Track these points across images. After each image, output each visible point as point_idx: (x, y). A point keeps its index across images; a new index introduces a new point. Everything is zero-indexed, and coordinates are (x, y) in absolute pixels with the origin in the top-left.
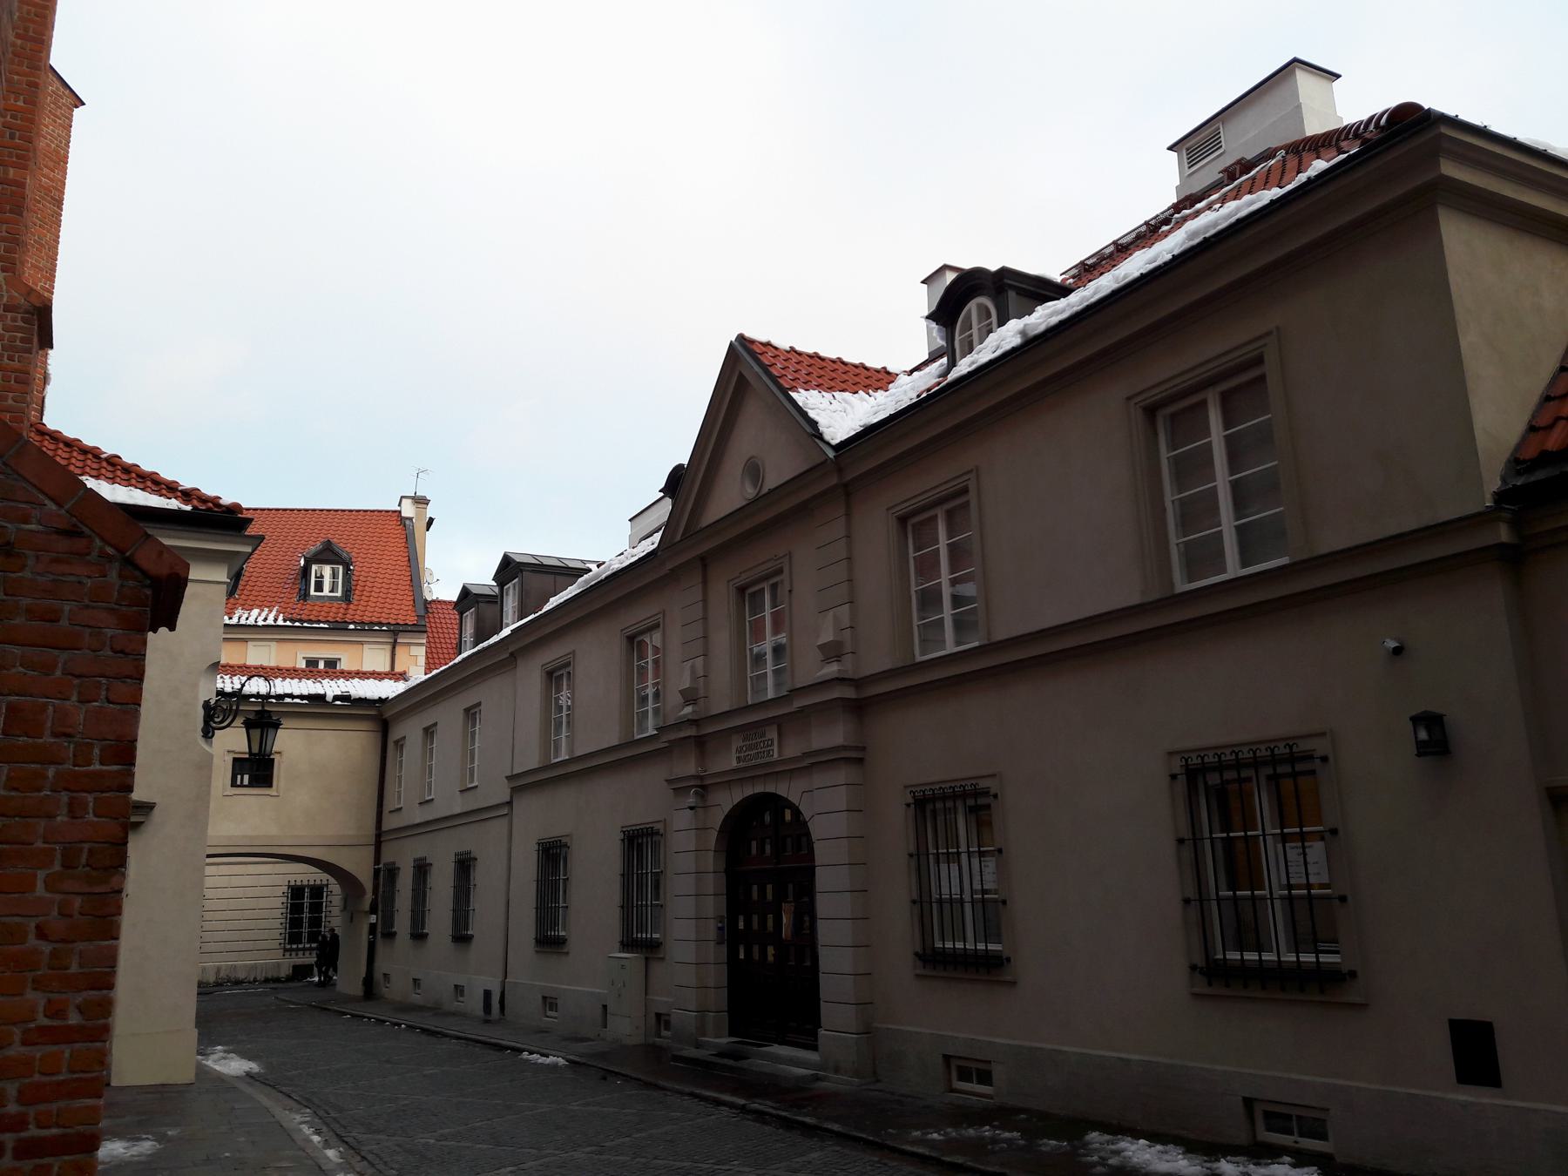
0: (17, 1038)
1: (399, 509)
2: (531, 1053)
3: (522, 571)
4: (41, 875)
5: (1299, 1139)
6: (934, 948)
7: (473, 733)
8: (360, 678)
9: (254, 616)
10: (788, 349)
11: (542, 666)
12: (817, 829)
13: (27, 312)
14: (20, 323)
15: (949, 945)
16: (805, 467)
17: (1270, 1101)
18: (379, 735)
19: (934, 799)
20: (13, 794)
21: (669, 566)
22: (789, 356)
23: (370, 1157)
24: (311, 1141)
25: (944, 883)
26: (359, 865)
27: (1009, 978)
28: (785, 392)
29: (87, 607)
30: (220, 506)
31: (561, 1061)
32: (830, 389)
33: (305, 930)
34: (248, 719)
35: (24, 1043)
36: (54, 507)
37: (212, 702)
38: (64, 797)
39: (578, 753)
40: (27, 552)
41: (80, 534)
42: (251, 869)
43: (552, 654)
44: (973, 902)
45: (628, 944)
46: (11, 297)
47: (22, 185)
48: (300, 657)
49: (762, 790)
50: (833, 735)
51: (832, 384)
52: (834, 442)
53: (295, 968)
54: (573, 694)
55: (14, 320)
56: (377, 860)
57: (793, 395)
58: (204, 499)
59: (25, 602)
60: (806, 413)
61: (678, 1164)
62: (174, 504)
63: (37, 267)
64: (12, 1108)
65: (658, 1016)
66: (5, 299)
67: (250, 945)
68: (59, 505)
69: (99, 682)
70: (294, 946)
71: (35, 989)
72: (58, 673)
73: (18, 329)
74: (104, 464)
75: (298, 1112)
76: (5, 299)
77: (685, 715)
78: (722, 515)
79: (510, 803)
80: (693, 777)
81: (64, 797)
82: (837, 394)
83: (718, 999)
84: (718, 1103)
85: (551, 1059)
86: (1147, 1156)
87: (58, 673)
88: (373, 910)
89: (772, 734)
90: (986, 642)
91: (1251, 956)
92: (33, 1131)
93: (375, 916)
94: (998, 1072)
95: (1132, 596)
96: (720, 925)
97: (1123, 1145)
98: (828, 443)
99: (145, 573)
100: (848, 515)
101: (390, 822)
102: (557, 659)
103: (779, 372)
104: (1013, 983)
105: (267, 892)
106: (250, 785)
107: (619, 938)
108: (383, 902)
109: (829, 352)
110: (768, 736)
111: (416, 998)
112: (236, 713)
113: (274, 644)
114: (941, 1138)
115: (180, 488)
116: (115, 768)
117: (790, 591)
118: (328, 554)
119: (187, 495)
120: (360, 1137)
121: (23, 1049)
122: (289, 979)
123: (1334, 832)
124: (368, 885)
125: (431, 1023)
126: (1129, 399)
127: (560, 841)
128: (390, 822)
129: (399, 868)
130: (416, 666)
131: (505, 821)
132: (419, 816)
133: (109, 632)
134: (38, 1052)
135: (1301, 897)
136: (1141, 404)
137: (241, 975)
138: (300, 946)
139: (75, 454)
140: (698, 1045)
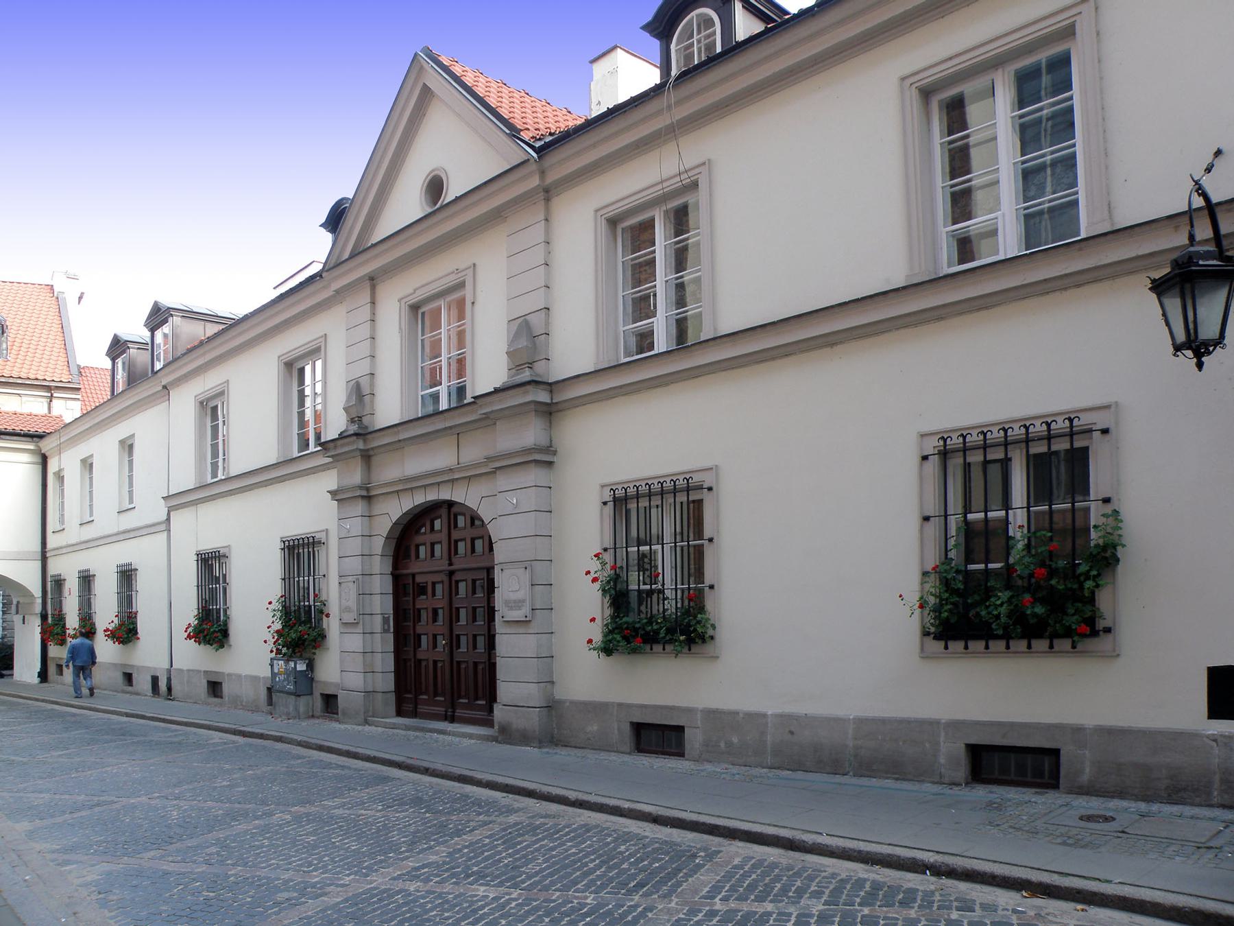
18: (39, 468)
19: (626, 499)
39: (170, 494)
101: (52, 541)
117: (473, 303)
126: (903, 79)
127: (219, 552)
129: (65, 580)
131: (166, 533)
136: (916, 85)
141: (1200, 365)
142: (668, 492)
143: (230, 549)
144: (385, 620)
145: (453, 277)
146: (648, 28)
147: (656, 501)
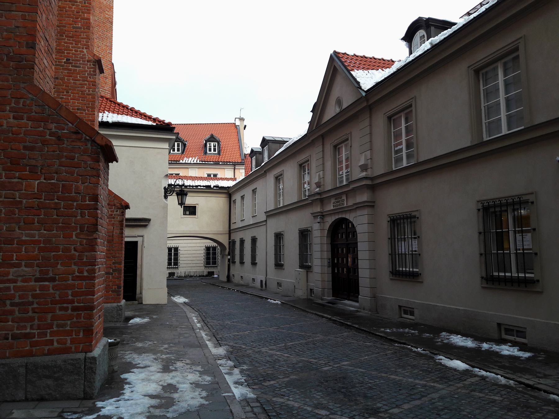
0: (70, 279)
1: (235, 122)
2: (271, 299)
3: (269, 143)
4: (74, 233)
5: (516, 338)
6: (396, 270)
7: (255, 198)
8: (222, 180)
9: (190, 160)
10: (353, 55)
12: (359, 229)
13: (94, 62)
14: (92, 66)
15: (401, 269)
16: (356, 99)
17: (507, 325)
18: (228, 199)
19: (397, 219)
20: (65, 210)
21: (311, 139)
22: (353, 57)
23: (209, 326)
24: (194, 321)
25: (400, 248)
26: (224, 240)
27: (421, 280)
28: (349, 71)
29: (82, 155)
30: (164, 123)
31: (279, 302)
32: (368, 69)
33: (211, 261)
34: (177, 192)
35: (72, 280)
36: (71, 125)
37: (167, 187)
38: (79, 211)
39: (285, 205)
40: (65, 139)
41: (79, 133)
42: (194, 241)
43: (276, 171)
44: (516, 254)
45: (302, 266)
46: (89, 58)
47: (89, 19)
48: (205, 173)
49: (345, 217)
50: (363, 197)
51: (369, 67)
52: (366, 90)
53: (209, 272)
54: (283, 184)
55: (90, 65)
56: (230, 239)
57: (352, 72)
58: (160, 121)
59: (65, 154)
60: (356, 79)
61: (300, 333)
62: (150, 123)
63: (107, 46)
64: (70, 297)
65: (311, 290)
66: (87, 59)
67: (194, 265)
68: (73, 125)
69: (87, 177)
70: (208, 266)
71: (75, 265)
72: (75, 175)
73: (91, 68)
74: (129, 111)
75: (194, 313)
76: (87, 59)
77: (317, 191)
78: (326, 121)
79: (266, 221)
80: (319, 212)
81: (79, 211)
82: (370, 71)
83: (329, 285)
84: (323, 317)
85: (277, 302)
86: (458, 340)
87: (75, 175)
88: (229, 254)
89: (344, 197)
90: (416, 162)
91: (502, 274)
92: (76, 304)
93: (229, 256)
94: (416, 312)
95: (467, 143)
96: (329, 261)
97: (452, 336)
98: (363, 90)
99: (98, 144)
100: (370, 117)
101: (233, 227)
103: (348, 64)
104: (422, 282)
105: (199, 248)
106: (189, 215)
107: (299, 265)
108: (232, 252)
109: (369, 55)
110: (343, 198)
111: (242, 282)
112: (174, 191)
113: (197, 169)
114: (390, 331)
115: (152, 118)
116: (93, 203)
117: (351, 146)
118: (212, 139)
119: (155, 120)
120: (209, 321)
121: (73, 282)
122: (206, 276)
123: (534, 229)
124: (227, 247)
125: (244, 290)
126: (469, 67)
128: (233, 227)
129: (245, 240)
130: (241, 175)
132: (241, 225)
133: (89, 163)
134: (76, 283)
135: (520, 253)
137: (192, 274)
138: (210, 266)
139: (121, 108)
140: (322, 299)
142: (405, 218)
145: (345, 137)
146: (404, 39)
147: (405, 221)
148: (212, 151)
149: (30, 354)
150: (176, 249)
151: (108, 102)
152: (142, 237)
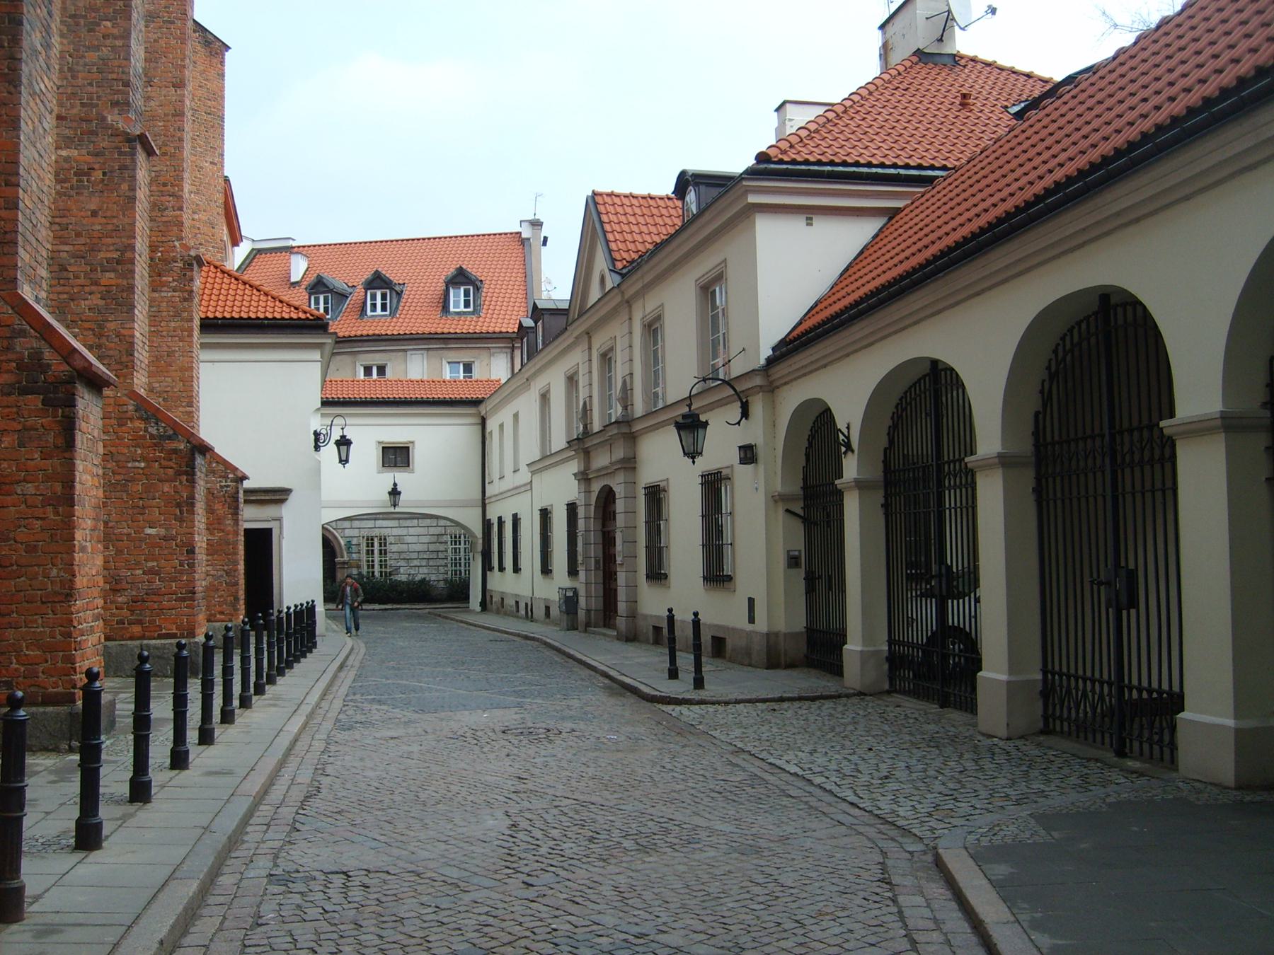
11: (696, 281)
26: (472, 521)
102: (707, 273)
109: (638, 191)
131: (530, 492)
141: (694, 462)
143: (732, 471)
144: (597, 562)
148: (462, 309)
149: (143, 637)
150: (383, 541)
151: (218, 274)
152: (278, 522)
